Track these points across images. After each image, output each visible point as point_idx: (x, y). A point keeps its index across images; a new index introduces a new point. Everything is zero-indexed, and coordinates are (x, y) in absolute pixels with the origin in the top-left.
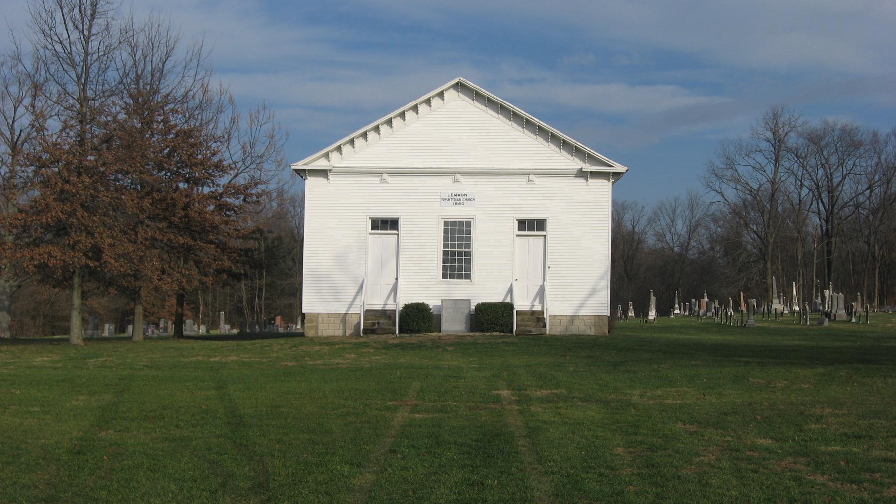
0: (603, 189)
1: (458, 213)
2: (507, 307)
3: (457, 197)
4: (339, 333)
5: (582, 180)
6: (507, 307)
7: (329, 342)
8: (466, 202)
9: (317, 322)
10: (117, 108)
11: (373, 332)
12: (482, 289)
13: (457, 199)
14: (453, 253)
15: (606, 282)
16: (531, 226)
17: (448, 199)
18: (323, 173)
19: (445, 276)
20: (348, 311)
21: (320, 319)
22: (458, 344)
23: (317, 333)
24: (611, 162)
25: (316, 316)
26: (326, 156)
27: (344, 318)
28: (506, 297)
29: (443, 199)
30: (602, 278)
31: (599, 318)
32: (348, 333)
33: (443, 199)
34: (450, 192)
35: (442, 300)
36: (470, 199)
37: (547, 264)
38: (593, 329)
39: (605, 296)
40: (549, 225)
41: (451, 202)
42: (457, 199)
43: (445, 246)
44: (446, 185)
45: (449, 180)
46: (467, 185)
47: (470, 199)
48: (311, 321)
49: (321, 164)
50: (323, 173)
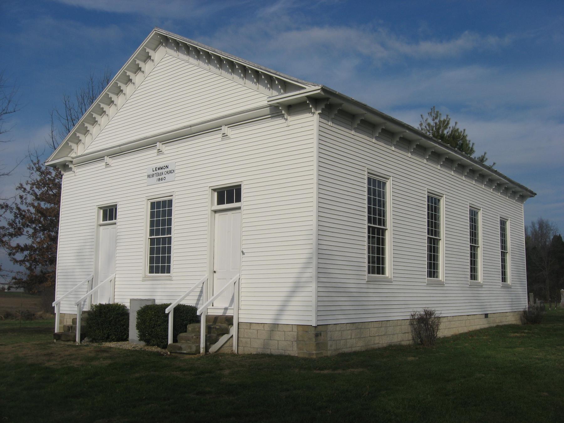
1: (160, 191)
5: (279, 122)
16: (229, 195)
25: (321, 308)
29: (149, 176)
36: (171, 172)
46: (171, 153)
47: (171, 172)
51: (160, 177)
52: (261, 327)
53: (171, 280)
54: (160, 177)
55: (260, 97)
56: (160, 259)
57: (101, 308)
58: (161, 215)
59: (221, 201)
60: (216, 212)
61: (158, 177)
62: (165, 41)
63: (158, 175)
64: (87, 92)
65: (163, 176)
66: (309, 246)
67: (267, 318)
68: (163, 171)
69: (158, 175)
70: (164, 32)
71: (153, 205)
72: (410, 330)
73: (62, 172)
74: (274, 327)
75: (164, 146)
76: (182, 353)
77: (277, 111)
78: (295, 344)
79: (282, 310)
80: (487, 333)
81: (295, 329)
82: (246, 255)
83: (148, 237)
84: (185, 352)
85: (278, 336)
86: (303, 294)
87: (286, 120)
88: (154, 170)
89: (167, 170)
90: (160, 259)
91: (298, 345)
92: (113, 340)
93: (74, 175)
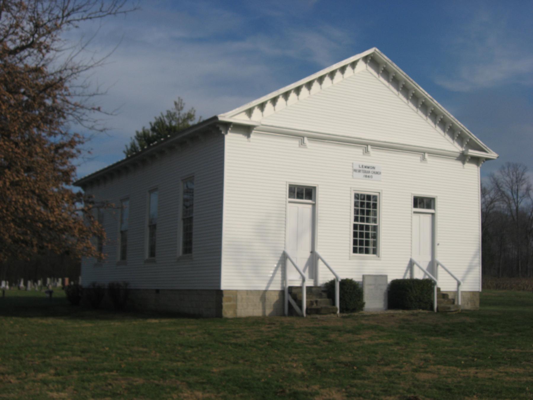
0: (473, 172)
1: (367, 187)
2: (428, 285)
3: (367, 169)
4: (257, 312)
5: (459, 163)
6: (428, 285)
7: (253, 322)
8: (374, 175)
9: (236, 300)
10: (14, 284)
11: (318, 311)
12: (390, 264)
13: (368, 171)
14: (362, 227)
15: (478, 261)
16: (423, 203)
17: (359, 171)
18: (246, 130)
19: (355, 251)
20: (268, 287)
21: (239, 297)
22: (375, 323)
23: (235, 313)
24: (488, 149)
25: (235, 293)
26: (249, 112)
27: (263, 295)
28: (406, 273)
29: (355, 171)
30: (475, 257)
31: (473, 293)
32: (268, 312)
33: (355, 171)
34: (361, 163)
35: (364, 277)
36: (377, 173)
37: (438, 240)
38: (469, 305)
39: (477, 272)
40: (439, 204)
41: (362, 175)
42: (368, 171)
43: (356, 219)
44: (355, 155)
45: (359, 151)
46: (375, 157)
47: (377, 173)
48: (230, 299)
49: (242, 119)
50: (246, 130)
51: (368, 175)
54: (368, 175)
55: (456, 148)
56: (365, 240)
58: (366, 207)
59: (415, 205)
60: (415, 212)
61: (365, 174)
63: (365, 172)
64: (296, 70)
65: (370, 174)
69: (365, 172)
80: (382, 362)
88: (361, 166)
90: (365, 240)
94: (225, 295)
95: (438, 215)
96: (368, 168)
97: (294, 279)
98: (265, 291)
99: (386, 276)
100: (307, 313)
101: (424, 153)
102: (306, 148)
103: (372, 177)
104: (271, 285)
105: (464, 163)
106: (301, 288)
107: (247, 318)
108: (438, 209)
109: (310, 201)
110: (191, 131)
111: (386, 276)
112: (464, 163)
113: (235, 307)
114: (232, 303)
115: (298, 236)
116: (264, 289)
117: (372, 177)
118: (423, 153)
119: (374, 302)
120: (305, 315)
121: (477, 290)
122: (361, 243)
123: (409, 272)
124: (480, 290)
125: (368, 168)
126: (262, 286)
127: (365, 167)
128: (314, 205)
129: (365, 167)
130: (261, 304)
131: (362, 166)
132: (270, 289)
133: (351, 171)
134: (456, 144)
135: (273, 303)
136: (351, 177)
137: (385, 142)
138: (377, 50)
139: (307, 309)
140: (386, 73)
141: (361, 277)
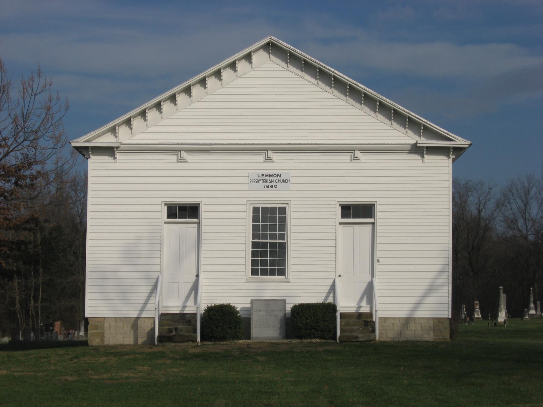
1: (270, 197)
3: (268, 178)
4: (129, 340)
5: (416, 158)
6: (328, 310)
7: (117, 352)
8: (278, 184)
9: (103, 328)
12: (299, 287)
14: (264, 245)
15: (447, 278)
16: (357, 212)
17: (258, 181)
18: (109, 151)
20: (140, 314)
21: (106, 325)
22: (271, 353)
23: (103, 341)
24: (451, 135)
26: (113, 130)
27: (135, 323)
28: (327, 297)
29: (252, 181)
30: (441, 273)
31: (439, 321)
32: (140, 341)
33: (252, 181)
35: (252, 301)
36: (284, 181)
42: (270, 180)
43: (255, 236)
44: (255, 164)
45: (259, 158)
46: (280, 164)
47: (284, 181)
48: (96, 327)
49: (107, 140)
51: (270, 184)
52: (397, 321)
53: (289, 282)
54: (270, 184)
55: (409, 138)
57: (302, 306)
60: (340, 224)
61: (266, 184)
62: (271, 48)
65: (273, 184)
66: (443, 259)
67: (402, 313)
68: (273, 178)
70: (275, 39)
71: (256, 210)
72: (106, 343)
73: (90, 156)
74: (407, 321)
75: (274, 155)
76: (358, 341)
77: (416, 150)
78: (431, 333)
79: (417, 306)
81: (431, 321)
82: (381, 263)
83: (251, 240)
84: (362, 340)
85: (412, 326)
86: (435, 295)
87: (423, 157)
88: (260, 175)
89: (279, 178)
91: (434, 332)
92: (242, 339)
93: (113, 161)
94: (91, 323)
95: (378, 224)
96: (271, 176)
97: (174, 305)
98: (137, 319)
99: (284, 301)
100: (158, 341)
101: (354, 151)
102: (187, 162)
103: (276, 186)
104: (144, 312)
105: (423, 157)
106: (195, 314)
107: (115, 347)
108: (378, 217)
109: (195, 220)
110: (441, 57)
111: (284, 301)
112: (423, 157)
113: (102, 335)
114: (99, 331)
115: (179, 259)
116: (135, 316)
117: (276, 186)
118: (349, 150)
119: (265, 330)
120: (156, 343)
121: (446, 316)
122: (273, 263)
123: (332, 295)
124: (450, 317)
125: (271, 176)
126: (134, 314)
127: (267, 176)
128: (199, 223)
129: (267, 176)
130: (132, 332)
131: (262, 175)
132: (142, 316)
133: (248, 182)
134: (410, 133)
135: (146, 332)
136: (247, 189)
137: (290, 144)
138: (273, 38)
139: (158, 336)
140: (292, 59)
141: (250, 302)
